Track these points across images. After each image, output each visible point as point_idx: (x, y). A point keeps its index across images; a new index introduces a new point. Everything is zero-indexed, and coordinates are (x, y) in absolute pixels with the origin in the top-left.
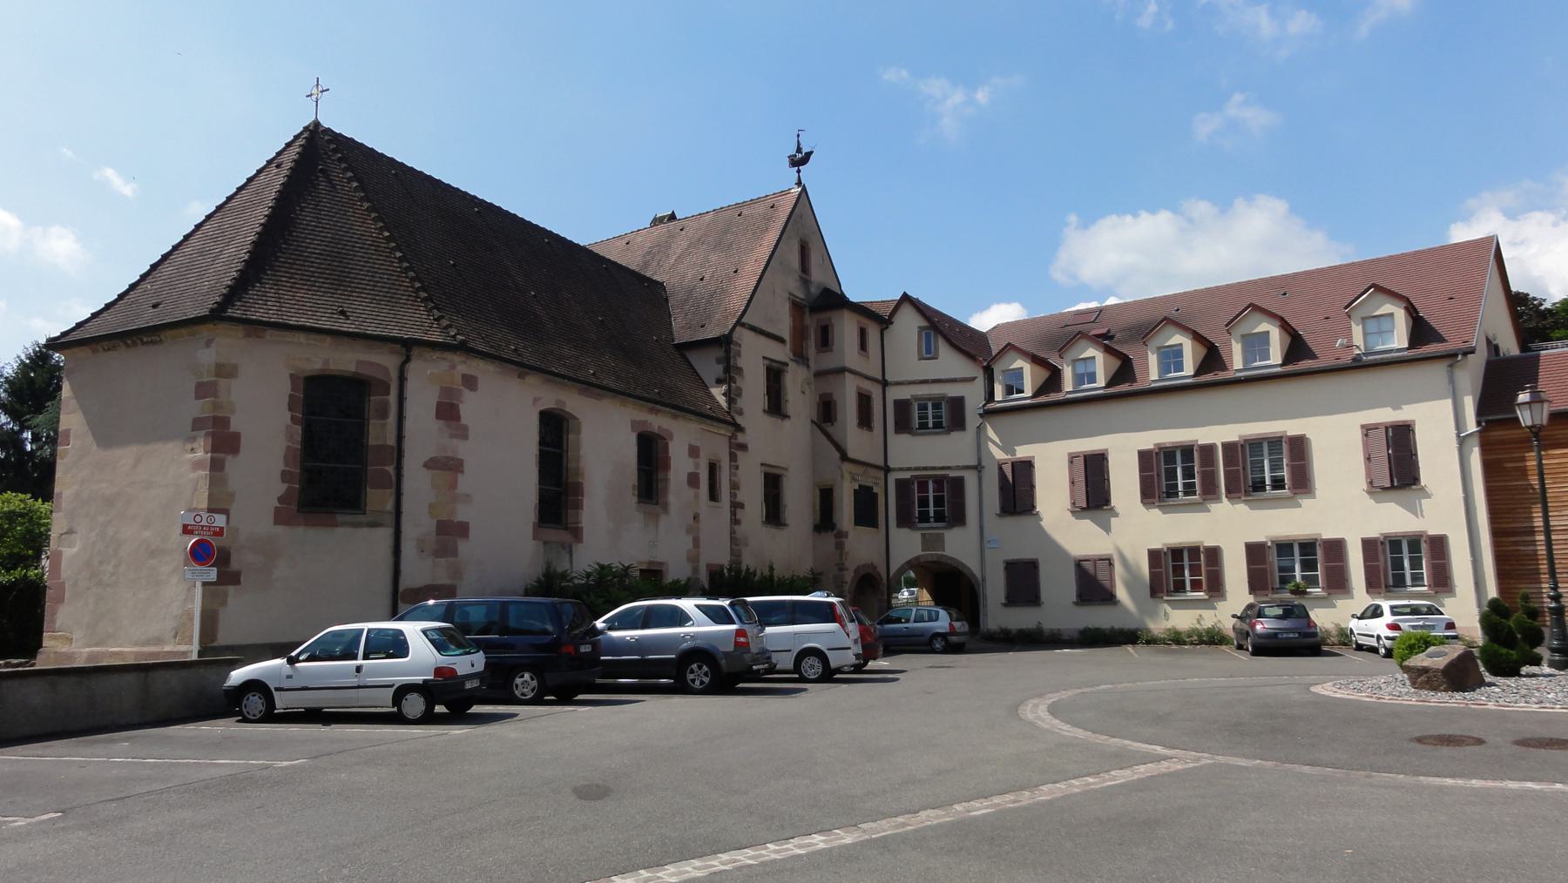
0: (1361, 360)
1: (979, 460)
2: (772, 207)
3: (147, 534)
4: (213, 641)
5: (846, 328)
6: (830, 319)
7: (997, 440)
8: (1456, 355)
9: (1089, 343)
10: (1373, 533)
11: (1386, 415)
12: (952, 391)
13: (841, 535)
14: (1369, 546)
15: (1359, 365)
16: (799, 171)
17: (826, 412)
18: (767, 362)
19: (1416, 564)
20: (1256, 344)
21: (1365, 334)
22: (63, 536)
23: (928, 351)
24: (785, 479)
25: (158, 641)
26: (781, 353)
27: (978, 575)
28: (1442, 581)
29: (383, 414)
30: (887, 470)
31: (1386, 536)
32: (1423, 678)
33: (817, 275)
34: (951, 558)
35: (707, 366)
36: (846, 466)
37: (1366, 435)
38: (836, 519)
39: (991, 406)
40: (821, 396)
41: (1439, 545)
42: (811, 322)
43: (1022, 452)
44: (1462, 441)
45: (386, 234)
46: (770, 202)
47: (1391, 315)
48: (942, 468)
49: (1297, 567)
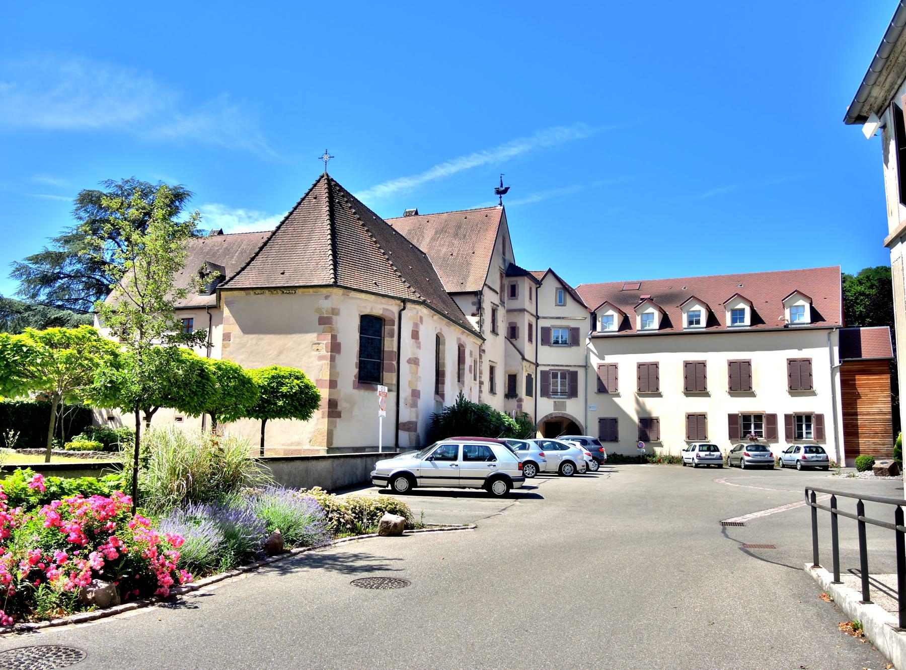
0: (788, 327)
1: (586, 363)
2: (487, 216)
4: (331, 445)
5: (524, 286)
6: (517, 281)
7: (596, 352)
8: (833, 329)
9: (648, 304)
10: (790, 412)
11: (795, 354)
12: (573, 324)
13: (520, 400)
14: (788, 417)
15: (786, 329)
16: (501, 197)
17: (513, 332)
18: (492, 305)
19: (808, 427)
20: (738, 315)
21: (791, 314)
23: (560, 301)
24: (496, 369)
25: (299, 444)
26: (497, 301)
27: (584, 427)
28: (820, 434)
29: (392, 336)
30: (537, 365)
31: (796, 414)
32: (880, 472)
33: (508, 257)
34: (569, 415)
35: (466, 305)
36: (525, 363)
37: (789, 364)
38: (518, 392)
39: (595, 334)
40: (510, 324)
41: (820, 418)
42: (507, 281)
43: (610, 359)
44: (833, 370)
45: (374, 239)
46: (484, 212)
47: (804, 306)
48: (567, 366)
49: (753, 426)
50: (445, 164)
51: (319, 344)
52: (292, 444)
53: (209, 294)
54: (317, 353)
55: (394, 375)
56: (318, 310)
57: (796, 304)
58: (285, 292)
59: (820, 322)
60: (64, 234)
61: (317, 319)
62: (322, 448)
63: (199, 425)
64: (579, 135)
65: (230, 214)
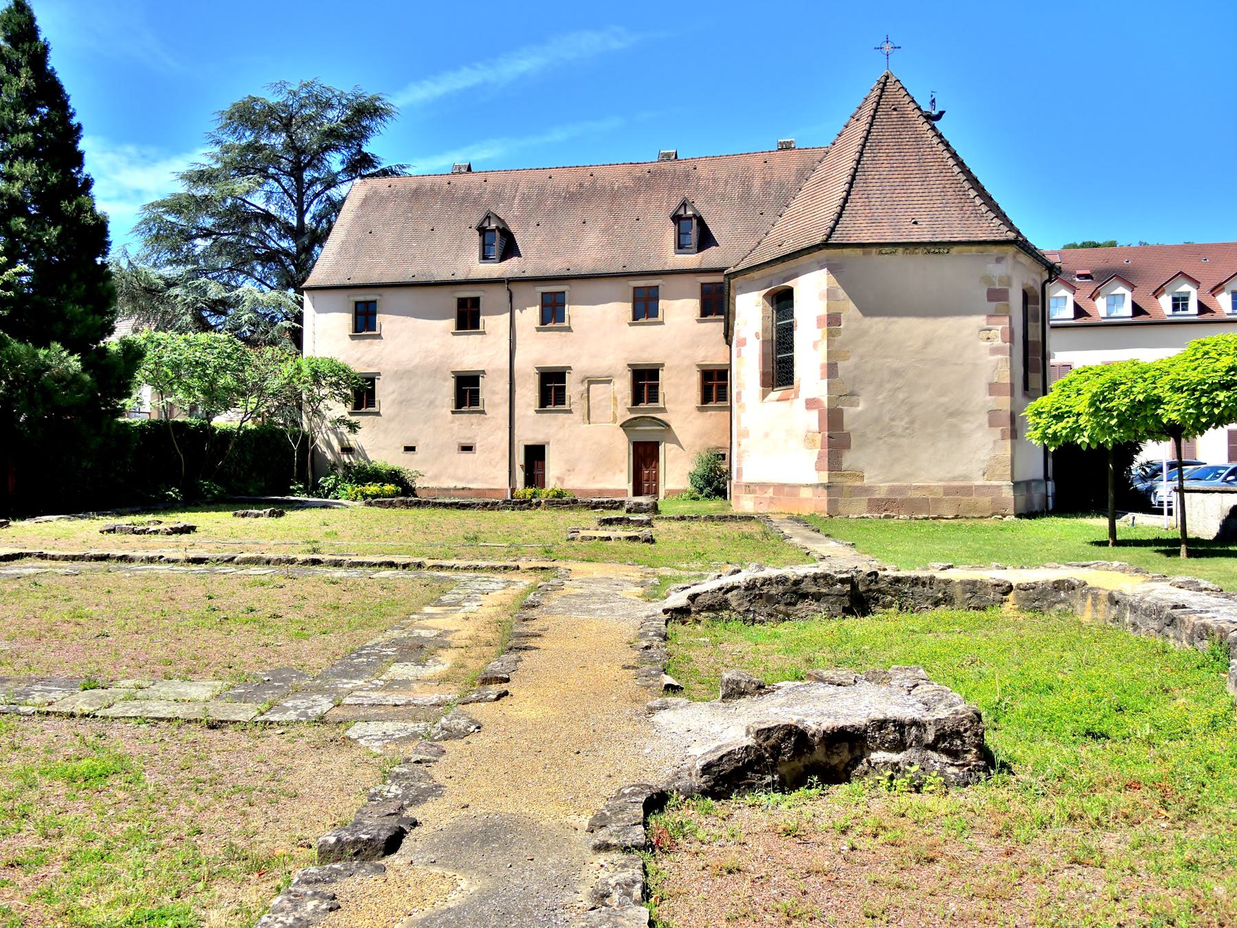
3: (944, 399)
22: (843, 398)
25: (965, 478)
29: (1037, 321)
47: (1124, 295)
50: (425, 82)
51: (990, 330)
52: (954, 479)
53: (497, 260)
54: (988, 343)
55: (1040, 376)
56: (987, 279)
57: (1114, 293)
58: (933, 250)
59: (1142, 316)
60: (197, 168)
61: (985, 292)
62: (1004, 483)
63: (504, 456)
64: (615, 45)
65: (114, 152)
